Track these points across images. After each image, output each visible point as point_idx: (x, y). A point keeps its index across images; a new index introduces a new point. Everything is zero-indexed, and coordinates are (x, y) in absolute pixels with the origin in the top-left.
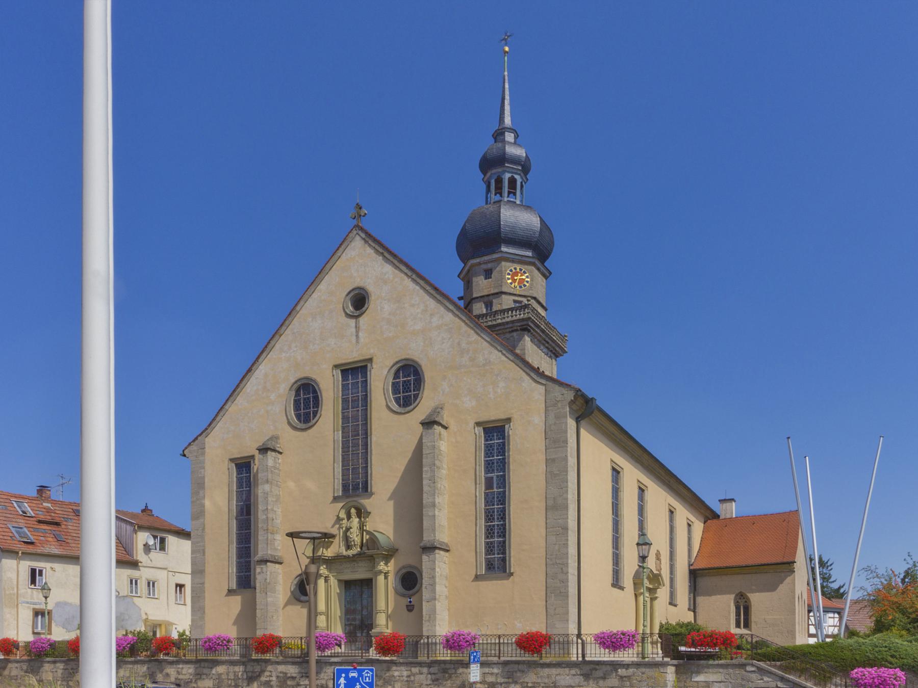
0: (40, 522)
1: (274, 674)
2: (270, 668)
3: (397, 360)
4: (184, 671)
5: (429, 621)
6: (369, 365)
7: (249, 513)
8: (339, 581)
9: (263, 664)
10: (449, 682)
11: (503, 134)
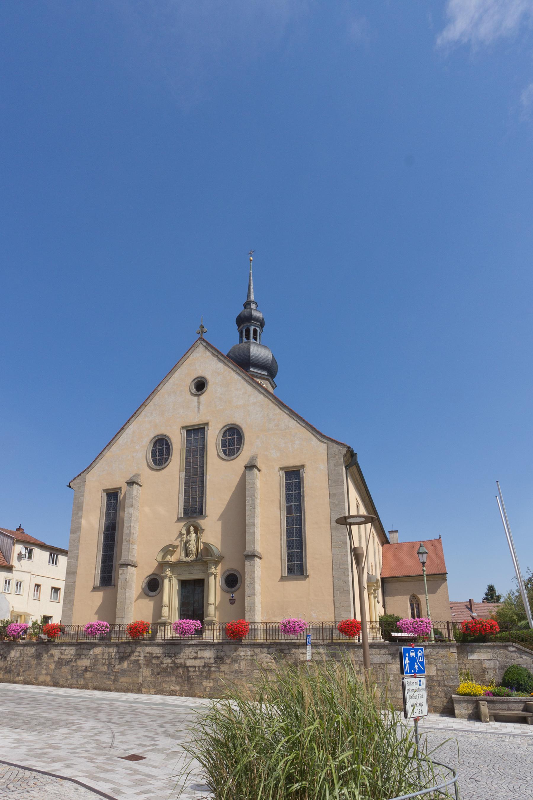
1: (142, 654)
2: (139, 649)
3: (225, 424)
4: (66, 652)
5: (250, 611)
6: (206, 427)
7: (114, 529)
8: (179, 580)
9: (134, 646)
10: (284, 660)
11: (250, 304)
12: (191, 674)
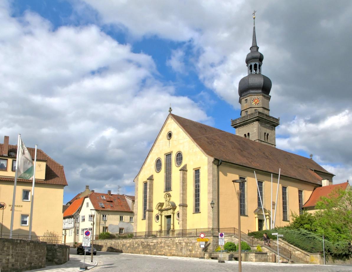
0: (107, 201)
12: (151, 247)
